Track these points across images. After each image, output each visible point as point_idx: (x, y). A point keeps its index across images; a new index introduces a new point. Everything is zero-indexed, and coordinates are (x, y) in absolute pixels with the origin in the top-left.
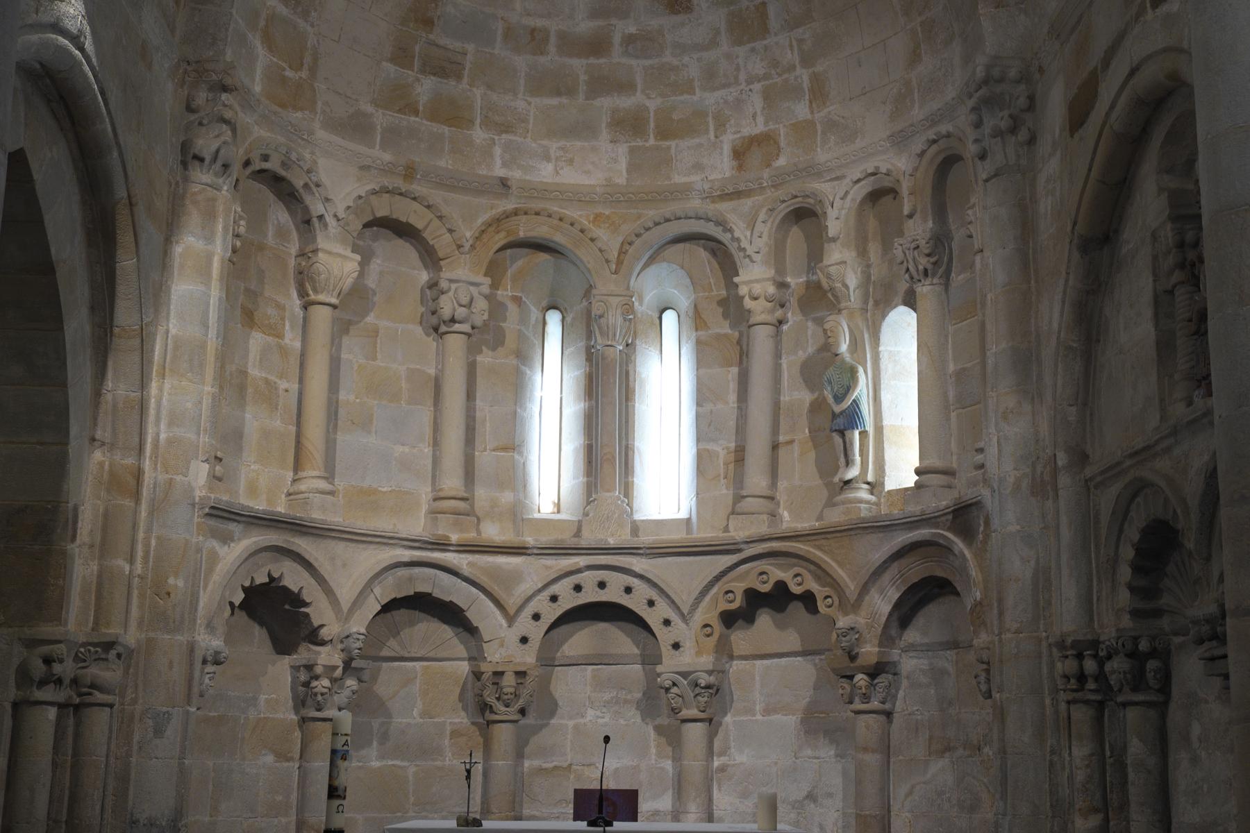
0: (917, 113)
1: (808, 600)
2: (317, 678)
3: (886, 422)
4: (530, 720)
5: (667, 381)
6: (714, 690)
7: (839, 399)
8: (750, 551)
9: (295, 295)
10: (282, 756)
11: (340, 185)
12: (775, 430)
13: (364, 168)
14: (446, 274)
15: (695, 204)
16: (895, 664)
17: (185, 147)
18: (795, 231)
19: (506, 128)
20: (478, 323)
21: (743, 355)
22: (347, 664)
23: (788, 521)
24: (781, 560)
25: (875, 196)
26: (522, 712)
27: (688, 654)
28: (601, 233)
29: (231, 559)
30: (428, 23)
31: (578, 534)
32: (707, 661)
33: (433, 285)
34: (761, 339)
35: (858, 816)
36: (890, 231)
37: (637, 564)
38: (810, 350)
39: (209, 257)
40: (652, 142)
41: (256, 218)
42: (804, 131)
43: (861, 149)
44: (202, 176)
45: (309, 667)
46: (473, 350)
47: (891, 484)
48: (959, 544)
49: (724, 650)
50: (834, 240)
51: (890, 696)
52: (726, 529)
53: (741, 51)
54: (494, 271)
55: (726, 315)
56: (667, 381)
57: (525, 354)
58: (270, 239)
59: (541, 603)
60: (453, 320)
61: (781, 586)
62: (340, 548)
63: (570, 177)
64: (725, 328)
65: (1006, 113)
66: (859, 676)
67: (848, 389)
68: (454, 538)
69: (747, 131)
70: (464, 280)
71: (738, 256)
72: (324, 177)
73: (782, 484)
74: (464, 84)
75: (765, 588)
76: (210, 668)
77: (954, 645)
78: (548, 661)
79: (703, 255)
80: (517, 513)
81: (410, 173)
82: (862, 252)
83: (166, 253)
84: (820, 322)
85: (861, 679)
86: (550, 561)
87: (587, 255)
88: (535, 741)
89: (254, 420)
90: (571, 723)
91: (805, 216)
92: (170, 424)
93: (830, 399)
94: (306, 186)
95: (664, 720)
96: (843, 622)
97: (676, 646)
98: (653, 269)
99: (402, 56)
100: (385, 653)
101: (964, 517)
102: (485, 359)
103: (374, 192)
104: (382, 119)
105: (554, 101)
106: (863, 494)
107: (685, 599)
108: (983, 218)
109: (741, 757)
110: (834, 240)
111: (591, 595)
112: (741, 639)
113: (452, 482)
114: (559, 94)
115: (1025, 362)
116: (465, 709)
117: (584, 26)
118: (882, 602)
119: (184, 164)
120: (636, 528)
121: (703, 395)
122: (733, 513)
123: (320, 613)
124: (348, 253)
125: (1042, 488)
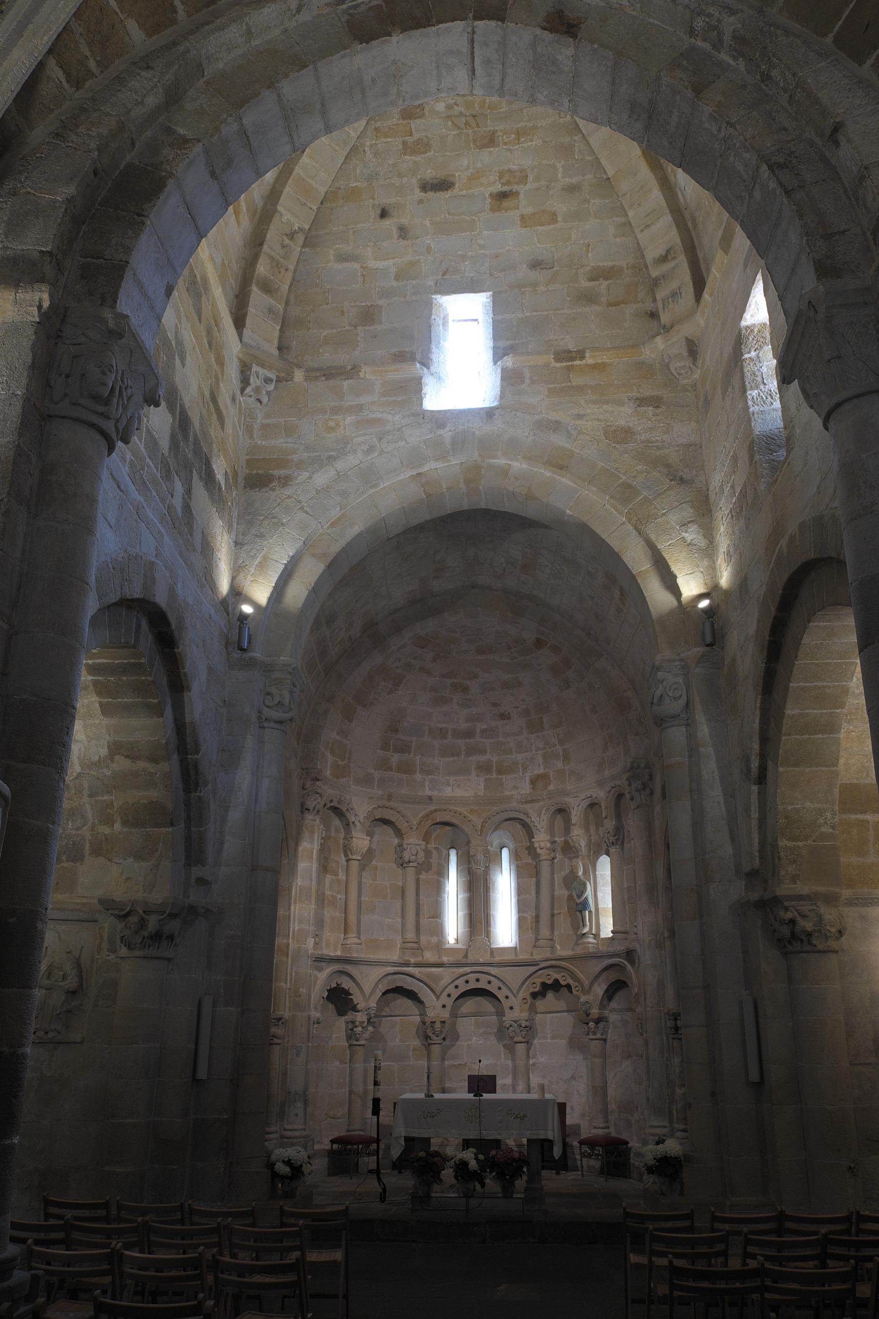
1: (568, 987)
2: (356, 1027)
3: (600, 906)
4: (447, 1043)
5: (504, 885)
6: (529, 1028)
7: (579, 897)
9: (343, 856)
10: (342, 1062)
11: (361, 807)
12: (552, 908)
13: (370, 798)
14: (406, 842)
15: (514, 804)
16: (606, 1018)
17: (303, 804)
18: (559, 818)
20: (420, 862)
21: (538, 874)
22: (369, 1020)
24: (556, 969)
25: (592, 805)
26: (444, 1039)
27: (517, 1012)
29: (323, 978)
30: (396, 731)
31: (466, 956)
34: (545, 867)
35: (593, 1087)
36: (599, 824)
37: (493, 970)
38: (567, 872)
39: (313, 849)
40: (495, 776)
41: (327, 825)
43: (585, 785)
44: (309, 817)
45: (353, 1022)
46: (418, 873)
48: (629, 967)
49: (533, 1010)
50: (575, 825)
51: (605, 1032)
52: (532, 955)
54: (426, 838)
55: (529, 854)
56: (504, 885)
57: (442, 873)
58: (333, 834)
59: (451, 989)
60: (409, 862)
61: (556, 981)
63: (459, 793)
65: (640, 782)
66: (591, 1023)
68: (412, 960)
69: (536, 772)
70: (414, 843)
71: (534, 829)
73: (556, 933)
74: (412, 755)
75: (550, 982)
76: (316, 1026)
77: (630, 1010)
78: (454, 1015)
79: (519, 826)
80: (439, 945)
81: (390, 798)
82: (587, 830)
83: (296, 850)
84: (570, 859)
85: (592, 1024)
86: (454, 970)
89: (328, 914)
90: (466, 1044)
91: (562, 811)
92: (299, 923)
93: (576, 897)
94: (347, 810)
95: (507, 1042)
96: (583, 999)
97: (511, 1008)
98: (496, 833)
99: (385, 747)
100: (384, 1013)
101: (630, 955)
102: (423, 876)
103: (374, 808)
104: (377, 775)
105: (452, 759)
106: (592, 940)
107: (515, 987)
108: (633, 823)
109: (542, 1059)
110: (575, 825)
111: (473, 985)
112: (540, 1004)
113: (411, 935)
114: (453, 755)
116: (418, 1038)
117: (464, 726)
118: (600, 990)
119: (302, 812)
120: (493, 952)
121: (520, 891)
122: (535, 946)
123: (357, 998)
124: (365, 837)
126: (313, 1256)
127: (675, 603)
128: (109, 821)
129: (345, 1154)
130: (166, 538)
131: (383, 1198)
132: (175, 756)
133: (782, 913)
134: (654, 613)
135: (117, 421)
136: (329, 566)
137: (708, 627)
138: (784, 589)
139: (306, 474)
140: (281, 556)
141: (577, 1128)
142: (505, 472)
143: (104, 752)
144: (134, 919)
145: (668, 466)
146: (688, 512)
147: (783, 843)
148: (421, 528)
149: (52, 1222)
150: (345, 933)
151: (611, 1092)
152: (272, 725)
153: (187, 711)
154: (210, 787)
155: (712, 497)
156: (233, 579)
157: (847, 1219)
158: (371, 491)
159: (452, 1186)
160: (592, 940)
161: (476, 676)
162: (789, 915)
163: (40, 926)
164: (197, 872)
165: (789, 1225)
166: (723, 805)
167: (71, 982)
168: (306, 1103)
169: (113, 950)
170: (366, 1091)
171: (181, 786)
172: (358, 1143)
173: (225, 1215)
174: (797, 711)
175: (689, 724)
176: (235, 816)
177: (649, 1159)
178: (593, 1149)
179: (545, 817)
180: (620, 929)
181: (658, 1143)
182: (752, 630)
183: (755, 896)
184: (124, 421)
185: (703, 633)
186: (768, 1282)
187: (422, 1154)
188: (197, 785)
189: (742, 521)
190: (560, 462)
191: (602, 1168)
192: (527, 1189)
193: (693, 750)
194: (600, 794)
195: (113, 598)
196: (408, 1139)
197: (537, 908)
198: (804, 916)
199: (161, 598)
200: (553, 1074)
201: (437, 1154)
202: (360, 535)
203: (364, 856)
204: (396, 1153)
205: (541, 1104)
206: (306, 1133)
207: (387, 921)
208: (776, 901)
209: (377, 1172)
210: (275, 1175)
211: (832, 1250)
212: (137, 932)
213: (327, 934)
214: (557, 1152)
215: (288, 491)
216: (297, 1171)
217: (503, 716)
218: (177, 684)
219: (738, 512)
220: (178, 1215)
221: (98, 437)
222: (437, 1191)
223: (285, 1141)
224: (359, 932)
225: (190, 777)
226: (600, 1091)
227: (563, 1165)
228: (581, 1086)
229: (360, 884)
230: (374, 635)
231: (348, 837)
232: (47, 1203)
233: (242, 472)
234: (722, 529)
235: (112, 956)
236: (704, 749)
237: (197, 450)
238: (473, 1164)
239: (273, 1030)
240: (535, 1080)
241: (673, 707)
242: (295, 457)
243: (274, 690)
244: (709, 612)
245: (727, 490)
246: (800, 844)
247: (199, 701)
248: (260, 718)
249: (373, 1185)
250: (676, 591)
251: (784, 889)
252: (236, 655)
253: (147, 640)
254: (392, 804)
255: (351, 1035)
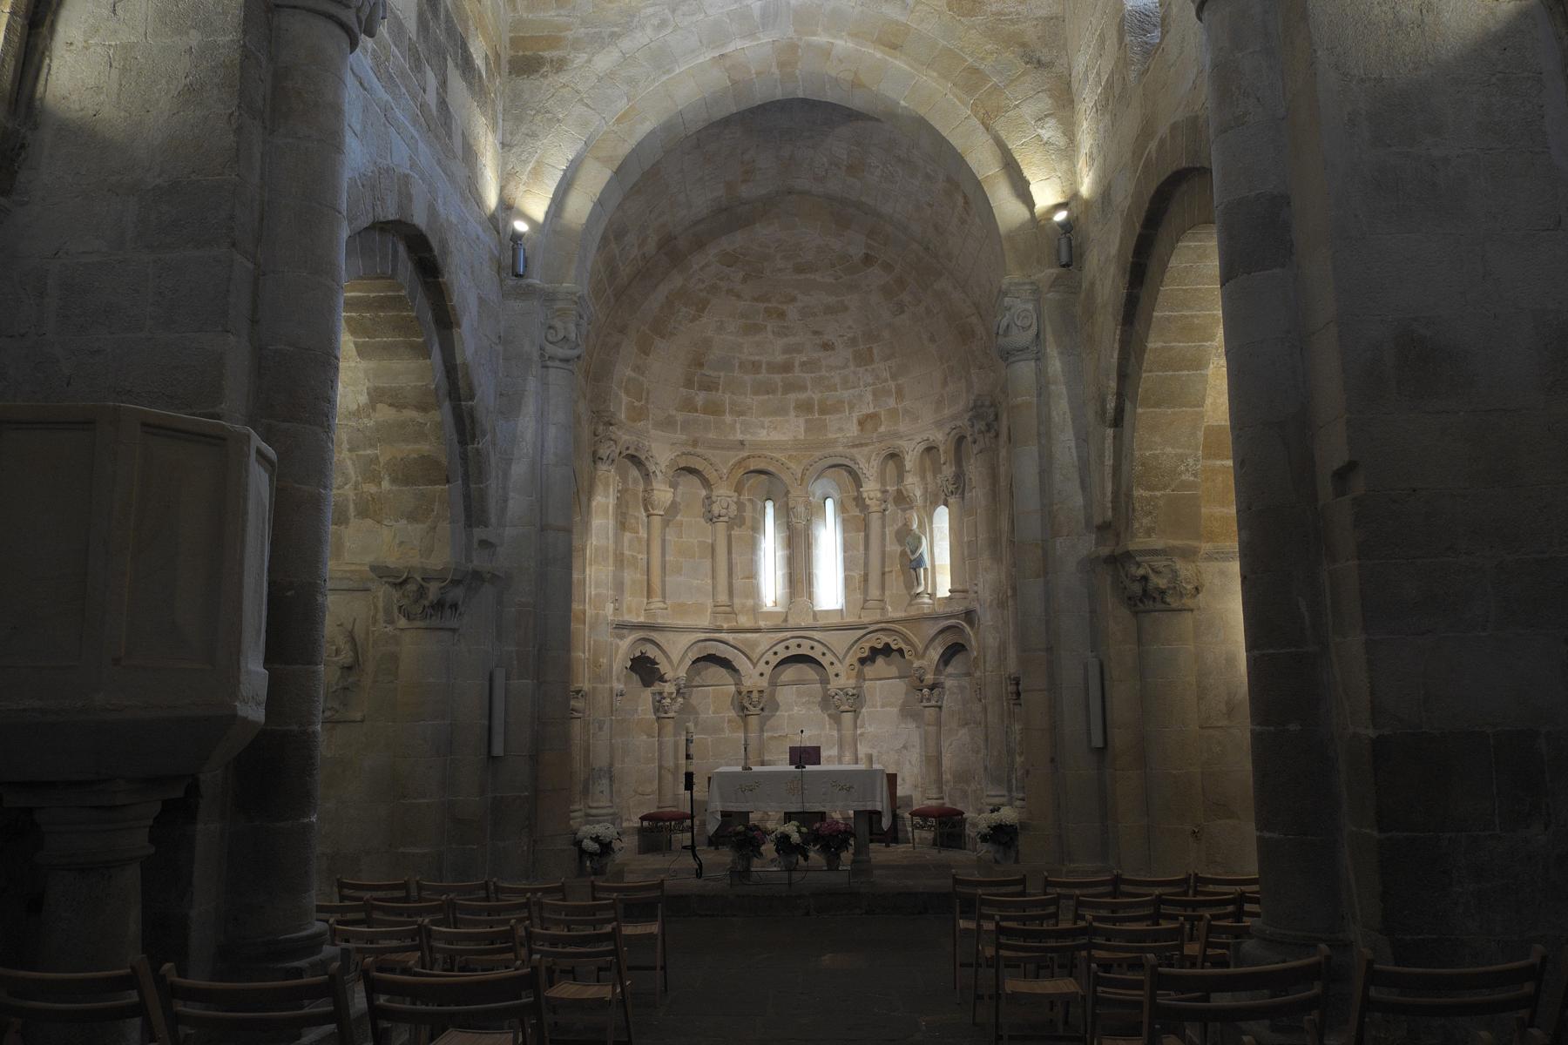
0: (947, 412)
1: (900, 651)
5: (828, 541)
6: (856, 696)
7: (913, 552)
8: (872, 628)
10: (649, 735)
11: (662, 455)
12: (883, 566)
14: (715, 493)
15: (840, 449)
19: (742, 413)
21: (866, 527)
23: (892, 613)
27: (843, 679)
28: (793, 465)
29: (625, 647)
30: (701, 365)
31: (786, 620)
32: (852, 682)
33: (708, 498)
34: (875, 520)
36: (936, 470)
37: (816, 635)
42: (893, 413)
43: (921, 426)
46: (730, 528)
47: (939, 595)
48: (968, 629)
49: (861, 676)
51: (940, 698)
53: (861, 370)
54: (738, 489)
56: (828, 541)
57: (757, 528)
59: (769, 656)
61: (887, 645)
62: (671, 635)
63: (775, 436)
64: (856, 512)
67: (917, 548)
68: (725, 626)
70: (724, 495)
72: (655, 453)
73: (887, 593)
77: (968, 674)
78: (773, 683)
79: (845, 474)
80: (755, 610)
81: (695, 443)
82: (923, 478)
83: (589, 505)
84: (904, 510)
87: (786, 478)
88: (772, 722)
89: (628, 576)
91: (894, 456)
95: (832, 711)
96: (916, 664)
99: (689, 383)
101: (969, 616)
104: (680, 417)
106: (927, 600)
107: (841, 652)
108: (975, 470)
111: (794, 651)
112: (869, 670)
113: (723, 598)
115: (994, 543)
117: (780, 358)
118: (935, 654)
120: (815, 614)
121: (847, 547)
123: (664, 667)
125: (1002, 605)
126: (628, 930)
127: (1027, 215)
128: (375, 478)
129: (657, 831)
130: (421, 145)
131: (699, 874)
132: (447, 404)
133: (1133, 570)
134: (1002, 228)
135: (359, 9)
136: (617, 172)
137: (1065, 243)
138: (1151, 203)
139: (585, 56)
140: (558, 159)
141: (908, 800)
142: (826, 52)
143: (363, 399)
144: (411, 587)
145: (1023, 45)
146: (1045, 103)
147: (1138, 492)
148: (726, 122)
149: (347, 903)
150: (649, 597)
151: (947, 762)
152: (557, 363)
153: (457, 351)
154: (488, 437)
155: (1075, 86)
156: (502, 189)
157: (1185, 881)
158: (664, 78)
159: (772, 861)
160: (927, 600)
161: (794, 299)
162: (1141, 572)
163: (320, 599)
164: (479, 533)
165: (1125, 888)
166: (1074, 450)
167: (346, 657)
168: (611, 779)
169: (391, 622)
170: (677, 766)
171: (455, 437)
172: (670, 820)
173: (535, 891)
174: (1160, 344)
175: (1040, 358)
176: (519, 470)
177: (983, 827)
178: (925, 821)
179: (875, 463)
180: (960, 588)
181: (992, 811)
182: (1113, 250)
183: (1105, 551)
184: (367, 10)
185: (1058, 251)
186: (1099, 940)
187: (741, 828)
188: (474, 437)
189: (1108, 117)
190: (893, 41)
191: (935, 839)
192: (853, 862)
193: (1043, 388)
194: (939, 437)
195: (365, 221)
196: (725, 814)
197: (866, 564)
198: (1157, 572)
199: (420, 219)
200: (884, 744)
201: (757, 828)
202: (653, 132)
203: (667, 511)
204: (712, 828)
205: (870, 774)
206: (617, 806)
207: (695, 582)
208: (1129, 555)
209: (692, 848)
210: (583, 852)
211: (1165, 909)
212: (416, 601)
213: (628, 599)
214: (886, 823)
215: (563, 78)
216: (606, 848)
217: (827, 346)
218: (445, 320)
219: (1103, 106)
220: (482, 894)
221: (338, 31)
222: (756, 865)
223: (590, 818)
224: (664, 597)
225: (465, 426)
226: (934, 761)
227: (893, 836)
228: (915, 755)
229: (664, 541)
230: (673, 251)
231: (648, 490)
232: (342, 886)
233: (506, 55)
234: (1085, 124)
235: (390, 628)
236: (1055, 387)
237: (451, 30)
238: (795, 838)
239: (573, 703)
240: (863, 750)
241: (1021, 338)
242: (569, 34)
243: (558, 324)
244: (1067, 226)
245: (1092, 76)
246: (1158, 494)
247: (470, 339)
248: (542, 356)
249: (689, 862)
250: (1028, 200)
251: (1138, 543)
252: (511, 281)
253: (406, 269)
254: (699, 450)
255: (659, 707)
